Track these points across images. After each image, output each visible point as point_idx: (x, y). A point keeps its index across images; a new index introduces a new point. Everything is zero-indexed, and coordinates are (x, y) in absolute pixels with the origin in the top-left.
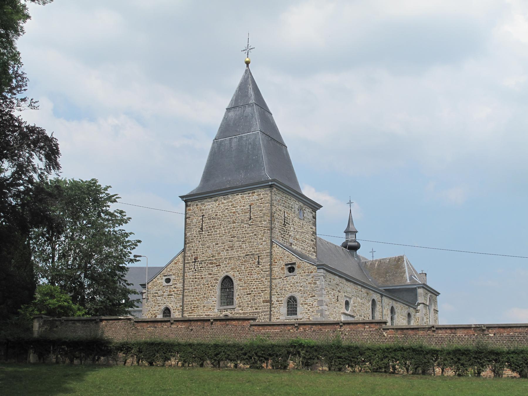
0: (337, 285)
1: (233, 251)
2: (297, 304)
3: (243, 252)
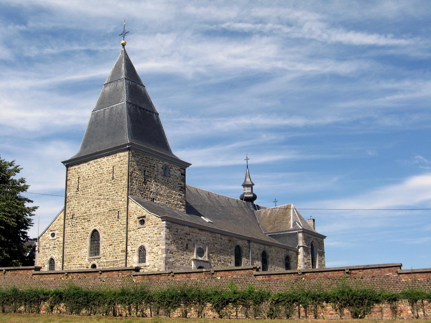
0: (187, 234)
1: (100, 207)
2: (146, 253)
3: (107, 208)
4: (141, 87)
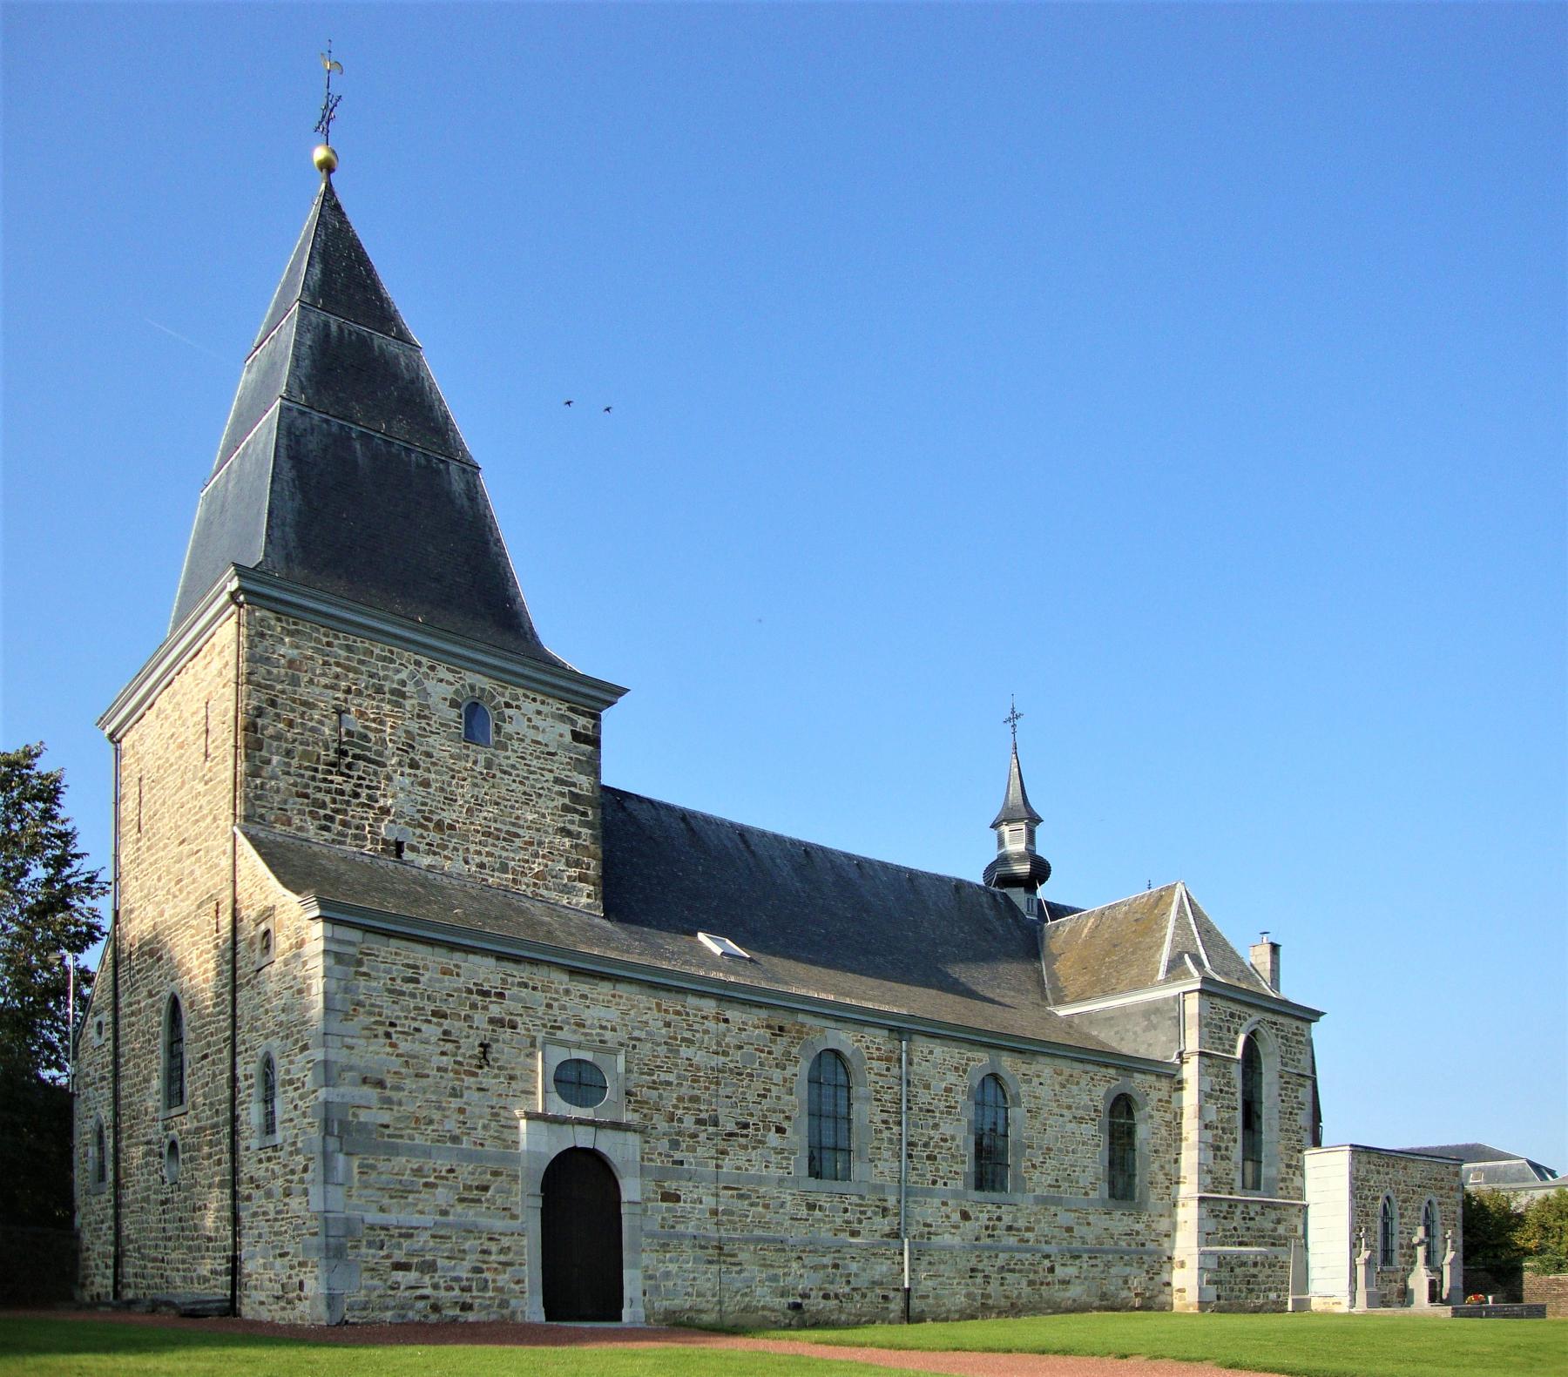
4: (394, 347)
